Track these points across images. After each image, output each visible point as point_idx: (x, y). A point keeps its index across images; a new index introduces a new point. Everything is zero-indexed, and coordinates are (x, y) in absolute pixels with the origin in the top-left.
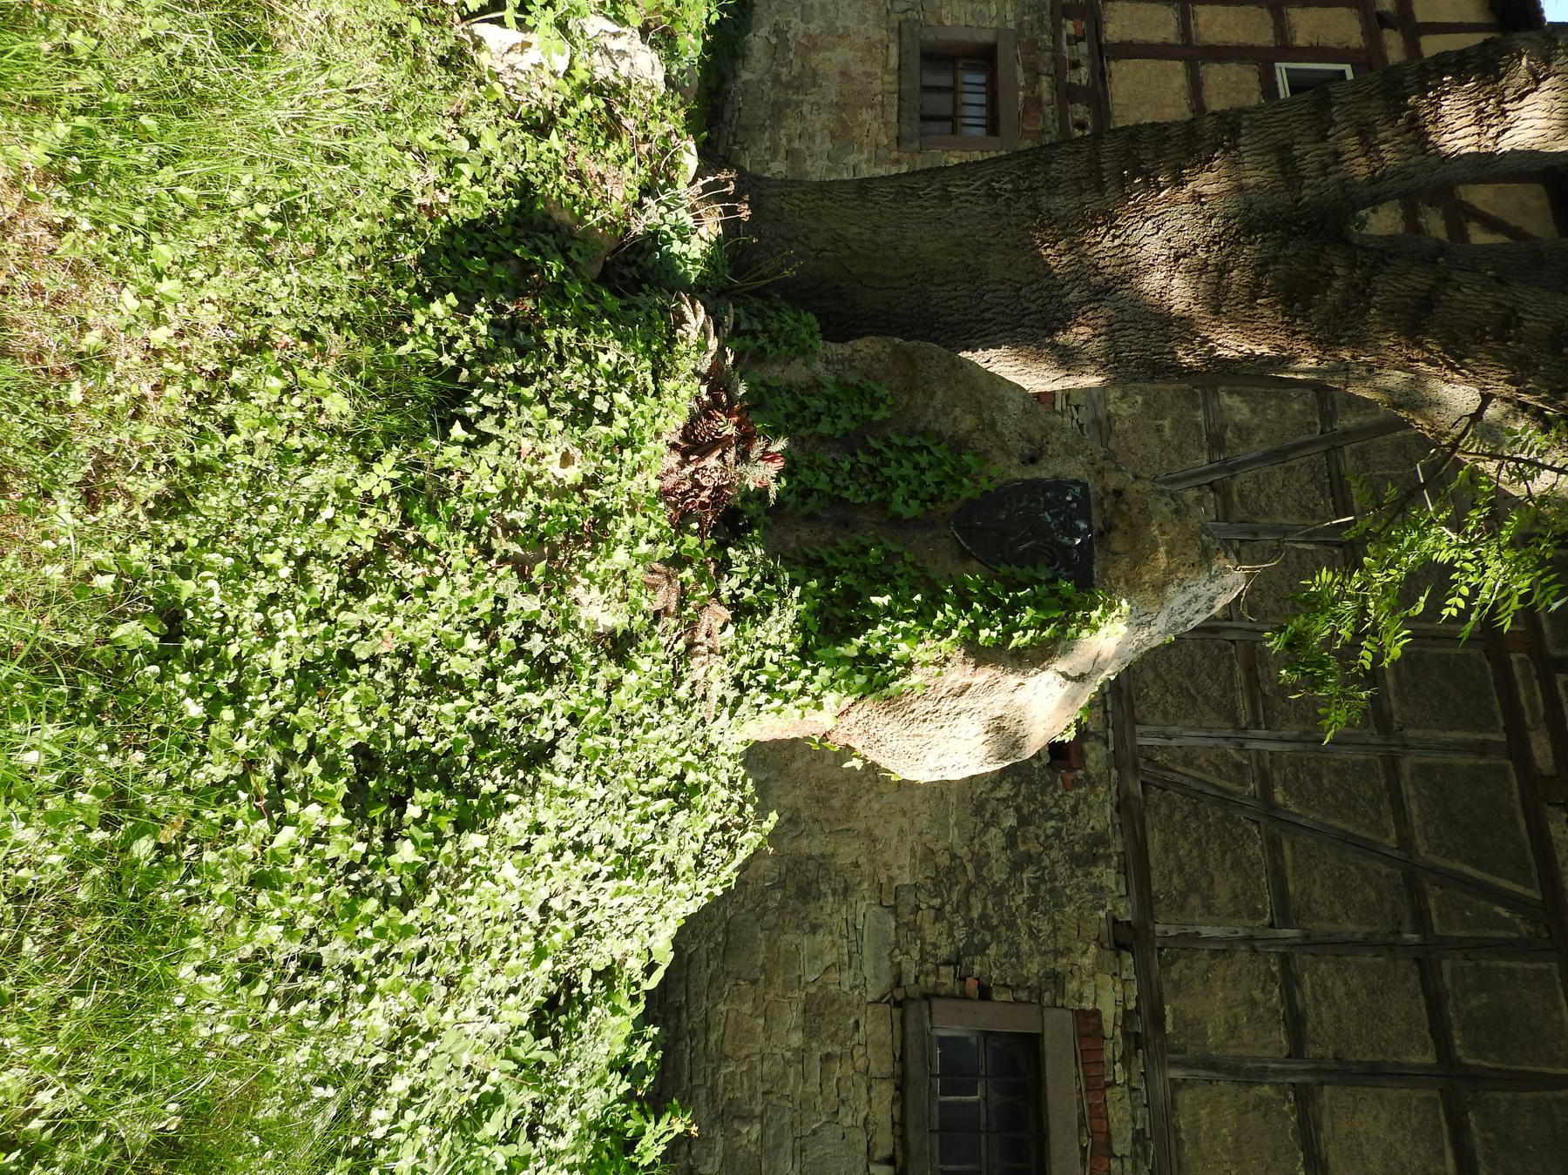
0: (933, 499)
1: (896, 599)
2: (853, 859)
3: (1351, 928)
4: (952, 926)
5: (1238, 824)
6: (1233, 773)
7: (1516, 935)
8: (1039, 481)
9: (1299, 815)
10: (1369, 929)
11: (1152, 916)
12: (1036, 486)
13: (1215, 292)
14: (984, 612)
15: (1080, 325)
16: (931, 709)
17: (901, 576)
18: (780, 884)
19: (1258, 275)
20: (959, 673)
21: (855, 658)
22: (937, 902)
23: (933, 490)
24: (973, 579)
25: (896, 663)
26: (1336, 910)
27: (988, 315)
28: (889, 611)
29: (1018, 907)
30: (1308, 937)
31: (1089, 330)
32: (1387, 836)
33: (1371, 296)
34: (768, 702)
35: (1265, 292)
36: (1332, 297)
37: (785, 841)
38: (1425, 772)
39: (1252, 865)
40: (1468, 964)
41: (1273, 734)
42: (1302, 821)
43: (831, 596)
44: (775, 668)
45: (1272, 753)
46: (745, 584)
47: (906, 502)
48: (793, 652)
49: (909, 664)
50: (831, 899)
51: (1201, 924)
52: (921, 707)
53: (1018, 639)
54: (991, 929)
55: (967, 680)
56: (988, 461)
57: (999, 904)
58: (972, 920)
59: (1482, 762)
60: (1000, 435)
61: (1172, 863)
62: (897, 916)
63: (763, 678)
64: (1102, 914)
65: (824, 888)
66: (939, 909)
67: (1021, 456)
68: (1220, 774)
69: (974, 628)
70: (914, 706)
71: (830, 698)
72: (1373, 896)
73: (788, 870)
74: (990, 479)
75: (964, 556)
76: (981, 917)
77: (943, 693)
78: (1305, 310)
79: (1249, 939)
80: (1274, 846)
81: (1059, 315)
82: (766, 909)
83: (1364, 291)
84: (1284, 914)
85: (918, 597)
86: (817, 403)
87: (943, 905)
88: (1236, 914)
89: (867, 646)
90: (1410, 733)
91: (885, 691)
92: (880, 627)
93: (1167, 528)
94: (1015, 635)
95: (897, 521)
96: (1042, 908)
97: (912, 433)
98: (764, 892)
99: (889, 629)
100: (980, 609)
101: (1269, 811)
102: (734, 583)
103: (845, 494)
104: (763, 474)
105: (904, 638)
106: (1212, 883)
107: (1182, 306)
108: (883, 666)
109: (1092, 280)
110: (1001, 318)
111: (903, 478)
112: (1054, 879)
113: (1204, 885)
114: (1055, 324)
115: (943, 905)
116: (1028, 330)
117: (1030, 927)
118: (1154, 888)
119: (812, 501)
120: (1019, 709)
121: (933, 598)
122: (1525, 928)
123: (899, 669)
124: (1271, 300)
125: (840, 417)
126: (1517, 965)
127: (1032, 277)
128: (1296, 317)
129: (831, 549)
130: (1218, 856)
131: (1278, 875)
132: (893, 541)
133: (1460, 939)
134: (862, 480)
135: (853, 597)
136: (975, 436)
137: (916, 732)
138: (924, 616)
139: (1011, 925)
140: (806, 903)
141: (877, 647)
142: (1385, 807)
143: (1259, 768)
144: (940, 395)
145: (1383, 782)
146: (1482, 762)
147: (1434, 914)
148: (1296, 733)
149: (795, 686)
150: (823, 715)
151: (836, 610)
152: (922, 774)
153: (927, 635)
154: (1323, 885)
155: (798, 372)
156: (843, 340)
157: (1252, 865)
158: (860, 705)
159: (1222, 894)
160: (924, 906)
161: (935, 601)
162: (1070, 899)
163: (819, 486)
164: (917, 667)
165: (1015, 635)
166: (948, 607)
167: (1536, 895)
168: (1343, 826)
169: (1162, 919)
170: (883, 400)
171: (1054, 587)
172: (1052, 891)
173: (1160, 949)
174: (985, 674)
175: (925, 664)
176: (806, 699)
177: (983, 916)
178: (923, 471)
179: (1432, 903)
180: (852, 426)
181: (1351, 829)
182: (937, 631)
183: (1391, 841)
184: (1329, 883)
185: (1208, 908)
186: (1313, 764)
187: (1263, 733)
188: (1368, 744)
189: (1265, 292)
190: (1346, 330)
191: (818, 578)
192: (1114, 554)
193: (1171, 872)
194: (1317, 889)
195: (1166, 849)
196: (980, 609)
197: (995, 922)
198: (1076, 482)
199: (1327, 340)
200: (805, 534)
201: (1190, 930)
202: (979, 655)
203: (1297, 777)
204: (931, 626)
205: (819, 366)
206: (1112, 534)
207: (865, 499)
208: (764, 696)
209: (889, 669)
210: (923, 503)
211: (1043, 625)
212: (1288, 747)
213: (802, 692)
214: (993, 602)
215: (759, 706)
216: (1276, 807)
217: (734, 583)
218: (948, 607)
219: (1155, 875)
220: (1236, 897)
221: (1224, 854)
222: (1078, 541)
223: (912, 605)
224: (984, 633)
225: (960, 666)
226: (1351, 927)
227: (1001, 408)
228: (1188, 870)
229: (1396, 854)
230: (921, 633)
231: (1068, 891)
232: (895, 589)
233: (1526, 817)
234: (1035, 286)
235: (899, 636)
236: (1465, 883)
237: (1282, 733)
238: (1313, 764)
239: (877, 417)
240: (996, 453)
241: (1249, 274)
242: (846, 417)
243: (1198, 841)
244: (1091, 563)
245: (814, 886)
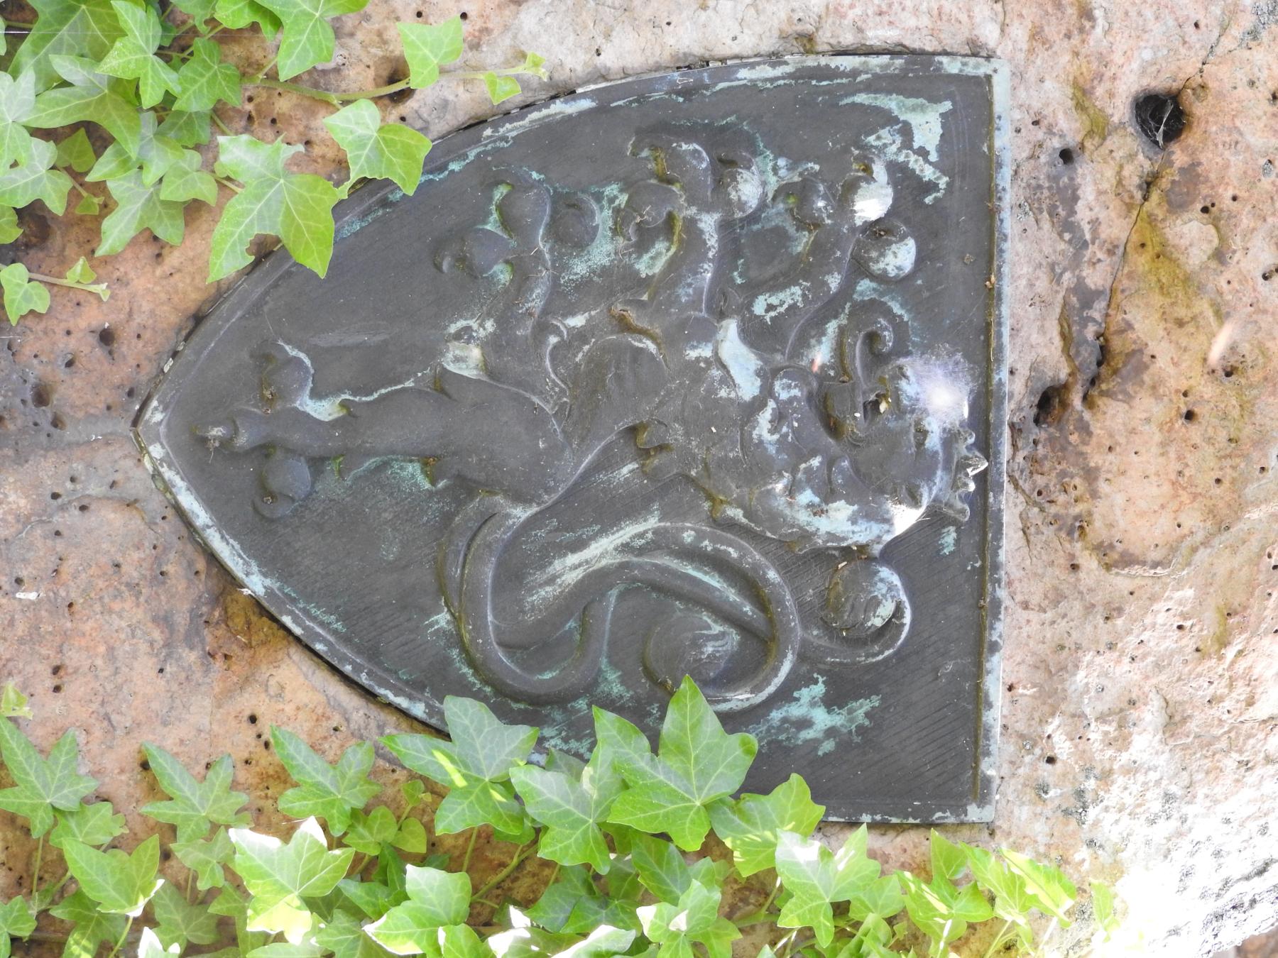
192: (1116, 558)
206: (1113, 417)
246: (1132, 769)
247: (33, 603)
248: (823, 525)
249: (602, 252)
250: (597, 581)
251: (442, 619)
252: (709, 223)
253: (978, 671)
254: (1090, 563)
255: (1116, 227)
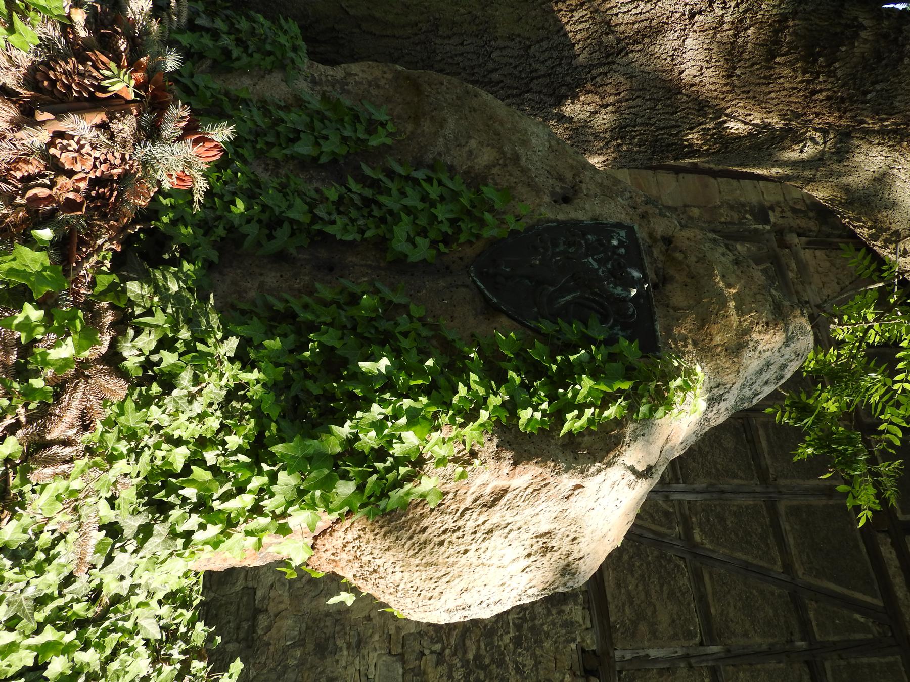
0: (447, 240)
1: (399, 365)
2: (365, 613)
3: (759, 641)
4: (451, 667)
5: (670, 561)
6: (663, 519)
7: (870, 636)
8: (576, 223)
9: (713, 551)
10: (770, 640)
11: (612, 644)
12: (573, 229)
13: (730, 53)
14: (523, 383)
15: (589, 92)
16: (450, 525)
17: (406, 335)
18: (300, 642)
19: (776, 32)
20: (488, 476)
21: (339, 456)
22: (438, 647)
23: (446, 228)
24: (506, 337)
25: (399, 461)
26: (747, 627)
27: (495, 76)
28: (388, 383)
29: (505, 646)
30: (729, 651)
31: (597, 99)
32: (775, 563)
33: (904, 46)
34: (202, 527)
35: (784, 49)
36: (860, 48)
37: (306, 601)
38: (794, 511)
39: (683, 594)
40: (843, 663)
41: (689, 487)
42: (715, 556)
43: (303, 364)
44: (208, 476)
45: (689, 502)
46: (166, 343)
47: (411, 241)
48: (240, 450)
49: (418, 462)
50: (345, 652)
51: (649, 648)
52: (435, 524)
53: (573, 423)
54: (484, 668)
55: (502, 483)
56: (514, 198)
57: (490, 644)
58: (468, 661)
59: (831, 502)
60: (524, 171)
61: (624, 597)
62: (404, 662)
63: (190, 492)
64: (573, 646)
65: (340, 642)
66: (440, 654)
67: (553, 194)
68: (654, 521)
69: (511, 408)
70: (425, 523)
71: (299, 518)
72: (771, 613)
73: (308, 628)
74: (518, 218)
75: (490, 310)
76: (475, 659)
77: (468, 503)
78: (829, 65)
79: (686, 657)
80: (697, 577)
81: (568, 79)
82: (286, 667)
83: (896, 39)
84: (710, 634)
85: (430, 362)
86: (294, 118)
87: (443, 649)
88: (674, 637)
89: (356, 438)
90: (781, 482)
91: (382, 503)
92: (375, 408)
93: (731, 280)
94: (569, 416)
95: (400, 265)
96: (525, 645)
97: (418, 164)
98: (285, 651)
99: (389, 411)
100: (518, 380)
101: (692, 548)
102: (147, 341)
103: (329, 230)
104: (182, 162)
105: (411, 424)
106: (654, 612)
107: (694, 71)
108: (379, 465)
109: (604, 39)
110: (508, 81)
111: (408, 210)
112: (533, 619)
113: (649, 614)
114: (563, 90)
115: (443, 649)
116: (536, 97)
117: (516, 663)
118: (612, 619)
119: (282, 234)
120: (575, 521)
121: (451, 366)
122: (875, 630)
123: (403, 470)
124: (791, 57)
125: (326, 138)
126: (874, 660)
127: (542, 33)
128: (818, 73)
129: (307, 299)
130: (658, 588)
131: (702, 599)
132: (394, 290)
133: (834, 643)
134: (354, 214)
135: (335, 364)
136: (495, 171)
137: (428, 559)
138: (438, 392)
139: (501, 663)
140: (323, 658)
141: (370, 439)
142: (771, 540)
143: (682, 515)
144: (451, 123)
145: (768, 520)
146: (831, 502)
147: (814, 624)
148: (704, 485)
149: (246, 500)
150: (297, 535)
151: (310, 384)
152: (438, 614)
153: (444, 419)
154: (735, 608)
155: (275, 88)
156: (333, 63)
157: (683, 594)
158: (347, 523)
159: (664, 619)
160: (427, 652)
161: (455, 369)
162: (547, 635)
163: (292, 215)
164: (429, 466)
165: (569, 416)
166: (473, 377)
167: (878, 602)
168: (744, 557)
169: (619, 646)
170: (383, 125)
171: (614, 349)
172: (533, 629)
173: (620, 672)
174: (527, 475)
175: (442, 461)
176: (261, 521)
177: (478, 657)
178: (433, 204)
179: (812, 615)
180: (343, 150)
181: (750, 559)
182: (459, 412)
183: (778, 567)
184: (739, 604)
185: (654, 634)
186: (719, 509)
187: (681, 486)
188: (754, 492)
189: (784, 49)
190: (873, 83)
191: (284, 336)
192: (676, 309)
193: (624, 605)
194: (731, 610)
195: (618, 586)
196: (518, 380)
197: (487, 661)
198: (620, 225)
199: (851, 98)
200: (271, 279)
201: (642, 653)
202: (519, 446)
203: (708, 521)
204: (448, 405)
205: (302, 86)
206: (669, 287)
207: (358, 238)
208: (195, 520)
209: (388, 470)
210: (434, 244)
211: (606, 401)
212: (700, 497)
213: (257, 510)
214: (535, 370)
215: (188, 535)
216: (696, 545)
217: (147, 341)
218: (473, 377)
219: (612, 608)
220: (674, 621)
221: (662, 586)
222: (634, 292)
223: (421, 373)
224: (525, 414)
225: (492, 464)
226: (759, 640)
227: (525, 143)
228: (637, 602)
229: (783, 577)
230: (435, 416)
231: (545, 628)
232: (396, 353)
233: (864, 542)
234: (545, 44)
235: (403, 421)
236: (832, 596)
237: (695, 486)
238: (719, 509)
239: (374, 142)
240: (522, 190)
241: (767, 31)
242: (334, 139)
243: (642, 576)
244: (653, 321)
245: (331, 641)
246: (689, 352)
247: (407, 397)
248: (616, 292)
249: (562, 248)
250: (568, 302)
251: (536, 309)
252: (583, 242)
253: (653, 325)
254: (672, 311)
255: (662, 258)
